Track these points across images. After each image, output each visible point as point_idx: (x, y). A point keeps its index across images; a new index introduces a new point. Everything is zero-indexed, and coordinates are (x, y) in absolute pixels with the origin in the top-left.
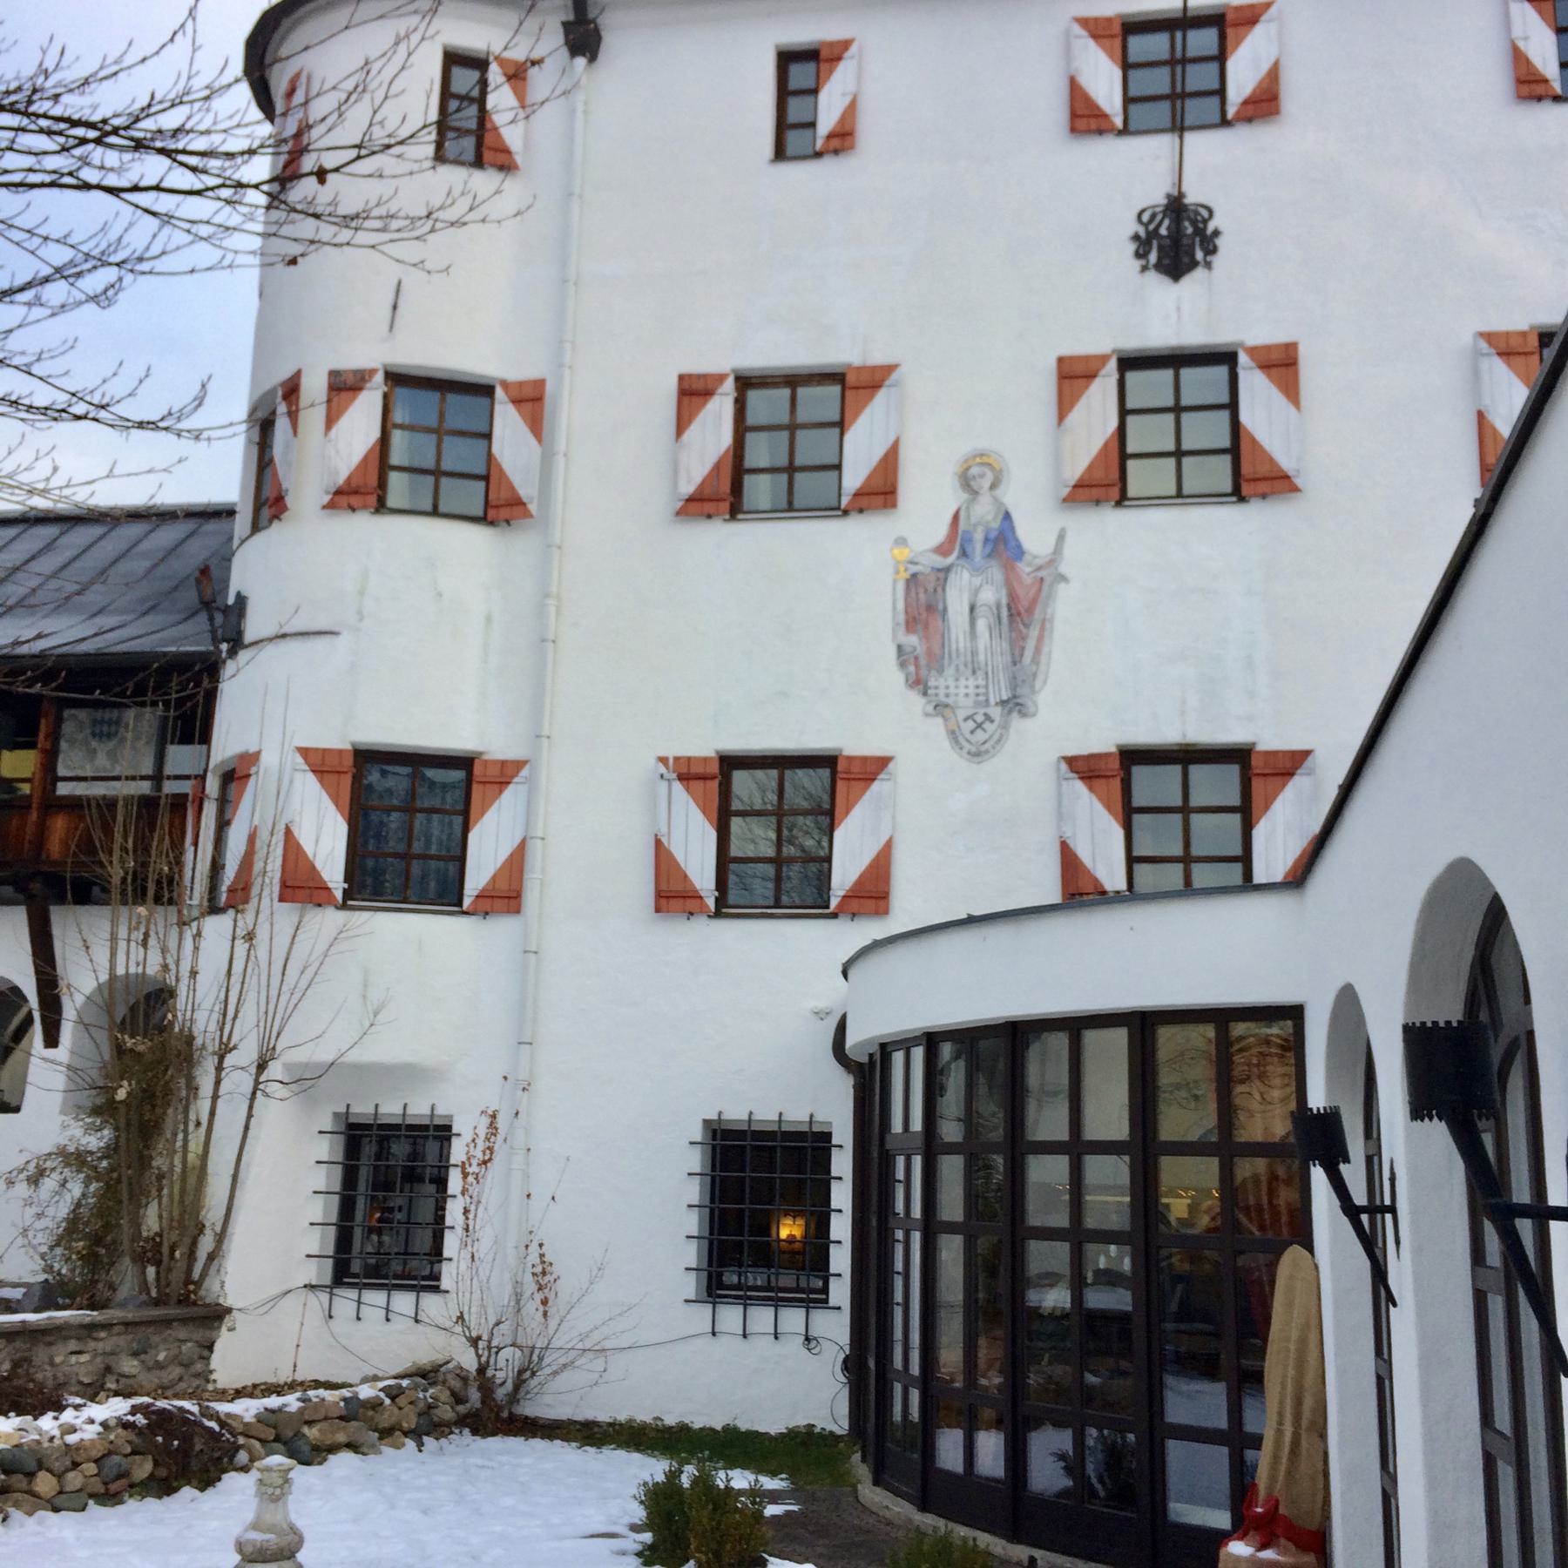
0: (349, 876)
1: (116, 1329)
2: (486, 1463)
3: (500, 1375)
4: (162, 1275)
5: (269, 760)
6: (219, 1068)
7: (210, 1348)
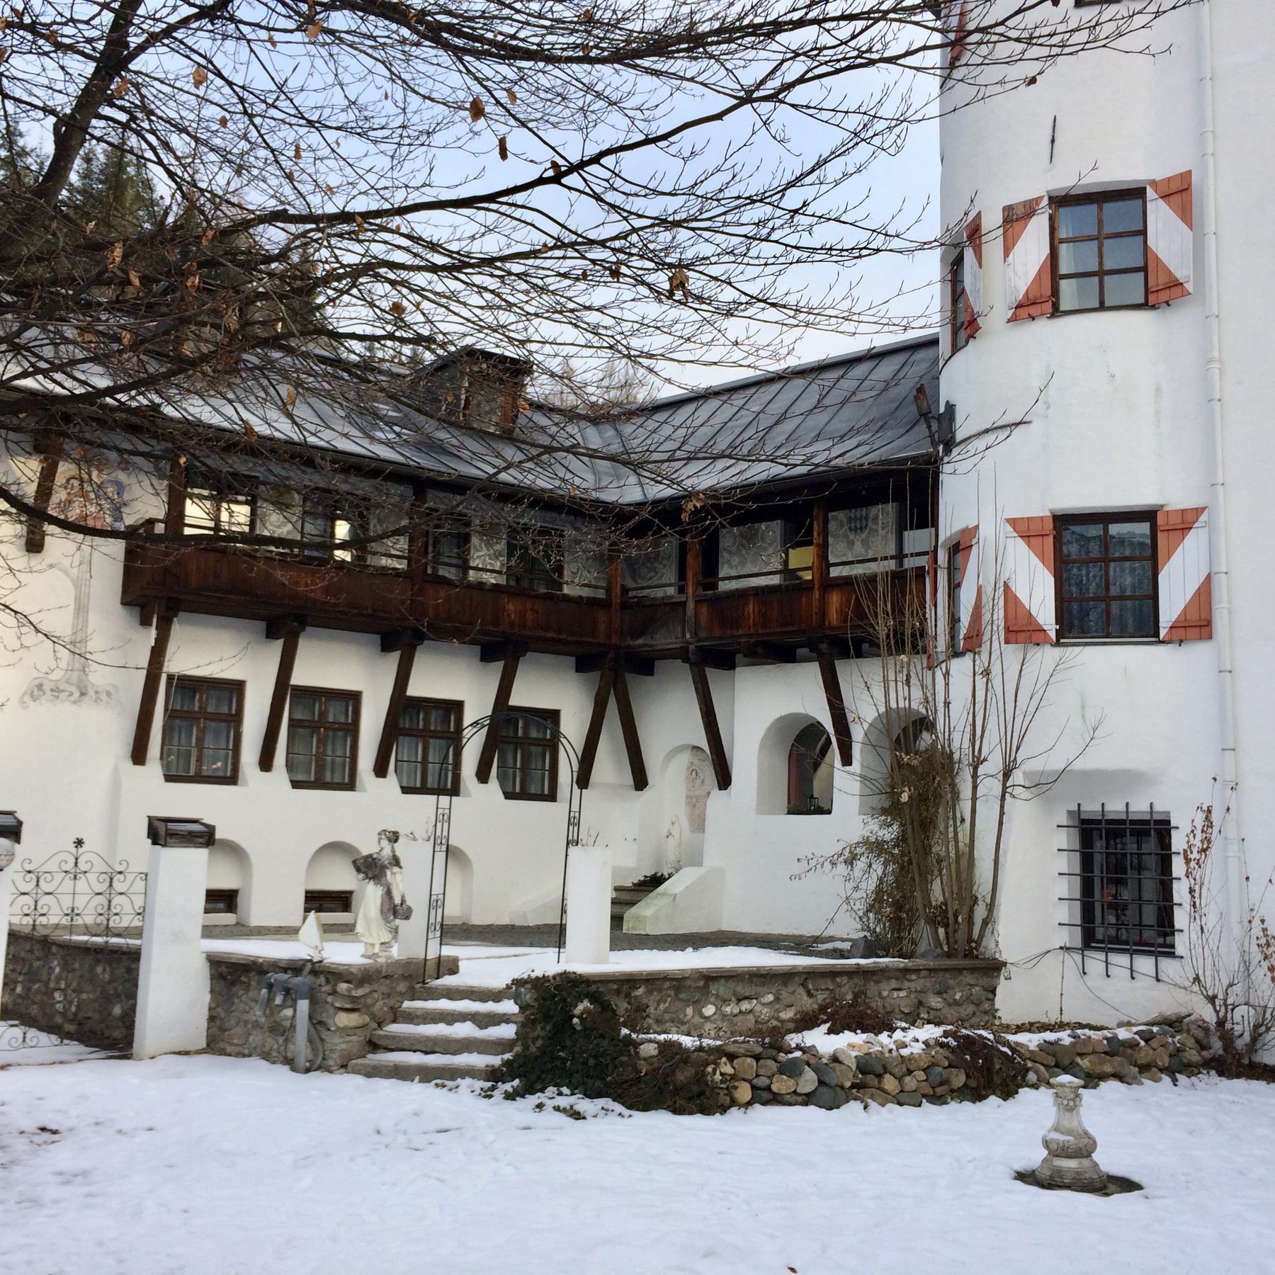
0: (1059, 619)
1: (923, 973)
2: (1236, 1099)
3: (1238, 1029)
4: (951, 935)
5: (986, 532)
6: (975, 776)
7: (993, 992)
